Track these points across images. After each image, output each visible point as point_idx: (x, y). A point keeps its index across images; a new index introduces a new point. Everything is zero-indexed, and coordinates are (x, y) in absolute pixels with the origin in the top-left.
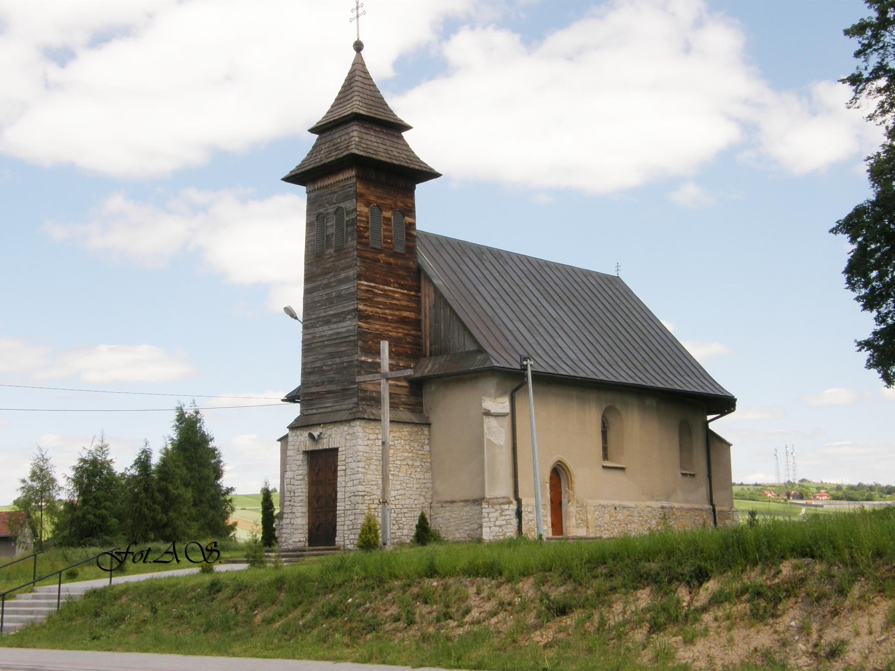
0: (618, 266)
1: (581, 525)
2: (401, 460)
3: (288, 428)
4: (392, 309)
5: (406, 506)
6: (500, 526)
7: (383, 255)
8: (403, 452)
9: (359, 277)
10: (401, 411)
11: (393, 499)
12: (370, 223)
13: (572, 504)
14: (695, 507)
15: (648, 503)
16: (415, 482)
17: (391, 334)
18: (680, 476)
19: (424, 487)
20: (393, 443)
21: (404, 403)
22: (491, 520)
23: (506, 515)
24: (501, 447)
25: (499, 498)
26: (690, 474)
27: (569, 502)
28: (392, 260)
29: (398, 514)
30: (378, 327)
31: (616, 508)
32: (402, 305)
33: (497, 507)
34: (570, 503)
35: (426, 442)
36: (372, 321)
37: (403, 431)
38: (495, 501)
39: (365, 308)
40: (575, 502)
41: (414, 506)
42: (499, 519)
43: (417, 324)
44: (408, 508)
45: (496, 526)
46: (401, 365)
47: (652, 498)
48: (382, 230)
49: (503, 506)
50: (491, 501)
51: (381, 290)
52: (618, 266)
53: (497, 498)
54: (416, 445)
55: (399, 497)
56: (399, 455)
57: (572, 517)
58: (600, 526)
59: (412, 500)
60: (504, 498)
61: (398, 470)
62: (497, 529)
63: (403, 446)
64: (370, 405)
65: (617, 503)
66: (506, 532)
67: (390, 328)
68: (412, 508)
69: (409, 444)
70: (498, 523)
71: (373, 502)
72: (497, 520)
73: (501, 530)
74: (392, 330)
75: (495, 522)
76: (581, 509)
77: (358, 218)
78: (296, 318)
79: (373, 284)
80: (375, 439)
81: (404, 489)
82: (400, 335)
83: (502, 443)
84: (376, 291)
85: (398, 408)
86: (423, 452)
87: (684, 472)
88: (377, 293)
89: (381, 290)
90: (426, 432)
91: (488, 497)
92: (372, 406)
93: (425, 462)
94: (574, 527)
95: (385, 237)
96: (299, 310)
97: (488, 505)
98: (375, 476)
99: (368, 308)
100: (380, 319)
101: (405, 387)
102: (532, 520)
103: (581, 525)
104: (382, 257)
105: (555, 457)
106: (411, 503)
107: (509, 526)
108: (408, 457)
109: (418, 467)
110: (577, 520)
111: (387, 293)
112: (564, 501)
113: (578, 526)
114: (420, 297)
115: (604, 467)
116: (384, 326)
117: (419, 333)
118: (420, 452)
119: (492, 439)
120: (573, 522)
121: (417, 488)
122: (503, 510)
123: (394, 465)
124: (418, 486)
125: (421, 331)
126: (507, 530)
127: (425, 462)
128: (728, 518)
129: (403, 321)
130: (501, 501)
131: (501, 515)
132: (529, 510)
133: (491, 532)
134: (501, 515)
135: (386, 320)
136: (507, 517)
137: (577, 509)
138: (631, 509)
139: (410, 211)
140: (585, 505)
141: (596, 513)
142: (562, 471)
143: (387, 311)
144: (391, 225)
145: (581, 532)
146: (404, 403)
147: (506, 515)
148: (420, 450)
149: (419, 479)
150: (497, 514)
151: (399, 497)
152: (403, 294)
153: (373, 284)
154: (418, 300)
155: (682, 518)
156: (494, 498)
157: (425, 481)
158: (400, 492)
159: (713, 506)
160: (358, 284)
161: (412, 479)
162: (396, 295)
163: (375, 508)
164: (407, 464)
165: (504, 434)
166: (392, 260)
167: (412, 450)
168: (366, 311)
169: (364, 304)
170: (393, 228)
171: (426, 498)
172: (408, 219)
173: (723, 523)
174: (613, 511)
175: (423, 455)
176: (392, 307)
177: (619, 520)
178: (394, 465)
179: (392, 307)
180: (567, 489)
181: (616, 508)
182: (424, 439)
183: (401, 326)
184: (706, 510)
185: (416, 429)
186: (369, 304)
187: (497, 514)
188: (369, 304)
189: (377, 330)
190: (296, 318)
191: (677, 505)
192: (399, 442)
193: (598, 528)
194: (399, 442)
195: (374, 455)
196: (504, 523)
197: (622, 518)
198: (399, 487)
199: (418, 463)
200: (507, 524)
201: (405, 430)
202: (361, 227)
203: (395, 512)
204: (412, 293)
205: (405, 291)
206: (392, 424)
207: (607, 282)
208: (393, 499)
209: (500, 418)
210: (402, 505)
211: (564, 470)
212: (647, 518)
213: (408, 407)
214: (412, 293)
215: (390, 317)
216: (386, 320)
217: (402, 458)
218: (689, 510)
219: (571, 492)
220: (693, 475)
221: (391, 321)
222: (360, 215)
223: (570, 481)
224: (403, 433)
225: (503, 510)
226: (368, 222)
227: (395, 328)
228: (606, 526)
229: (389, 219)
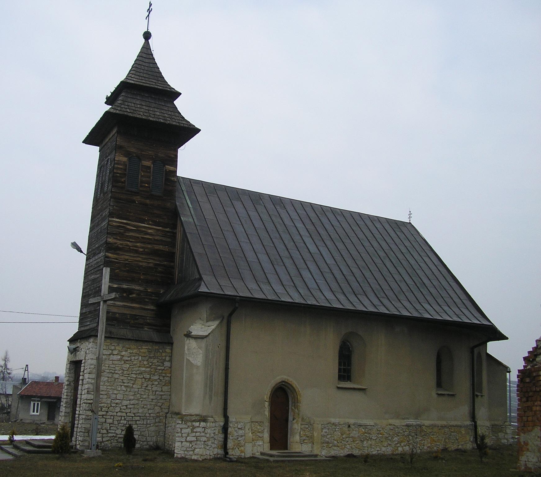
0: (410, 214)
1: (305, 441)
2: (136, 374)
3: (68, 341)
4: (144, 243)
5: (138, 414)
6: (191, 442)
7: (138, 197)
8: (139, 367)
9: (111, 215)
10: (146, 331)
11: (125, 407)
12: (127, 170)
13: (296, 422)
14: (451, 424)
15: (391, 421)
16: (151, 393)
17: (141, 264)
18: (436, 396)
19: (161, 399)
20: (129, 359)
21: (149, 324)
22: (184, 435)
23: (196, 432)
24: (198, 367)
25: (193, 415)
26: (448, 395)
27: (293, 420)
28: (148, 201)
29: (128, 421)
30: (127, 257)
31: (349, 426)
32: (155, 240)
33: (189, 424)
34: (295, 421)
35: (168, 358)
36: (121, 253)
37: (142, 349)
38: (188, 418)
39: (115, 241)
40: (300, 420)
41: (147, 415)
42: (190, 435)
43: (171, 256)
44: (140, 417)
45: (186, 441)
46: (149, 290)
47: (397, 416)
48: (140, 176)
49: (194, 423)
50: (185, 418)
51: (134, 226)
52: (410, 214)
53: (191, 415)
54: (155, 361)
55: (131, 406)
56: (135, 369)
57: (296, 433)
58: (328, 443)
59: (146, 409)
60: (197, 415)
61: (132, 382)
62: (188, 444)
63: (140, 362)
64: (112, 325)
65: (352, 421)
66: (195, 448)
67: (140, 259)
68: (145, 416)
69: (147, 360)
70: (188, 439)
71: (102, 409)
72: (188, 436)
73: (191, 446)
74: (142, 260)
75: (186, 437)
76: (307, 426)
77: (116, 166)
78: (82, 252)
79: (125, 221)
80: (110, 355)
81: (138, 400)
82: (151, 265)
83: (199, 364)
84: (128, 227)
85: (142, 328)
86: (163, 368)
87: (440, 392)
88: (128, 228)
89: (134, 226)
90: (168, 350)
91: (184, 414)
92: (114, 325)
93: (164, 377)
94: (297, 442)
95: (142, 182)
96: (84, 246)
97: (182, 421)
98: (105, 387)
99: (118, 241)
100: (130, 250)
101: (152, 310)
102: (242, 436)
103: (305, 441)
104: (137, 199)
105: (278, 378)
106: (145, 412)
107: (198, 442)
108: (145, 372)
109: (156, 380)
110: (300, 437)
111: (139, 229)
112: (290, 418)
113: (302, 442)
114: (176, 233)
115: (338, 388)
116: (133, 257)
117: (172, 264)
118: (159, 368)
119: (191, 359)
120: (297, 438)
121: (152, 399)
122: (194, 427)
123: (129, 378)
124: (154, 397)
125: (174, 262)
126: (196, 447)
127: (164, 377)
128: (501, 431)
129: (155, 253)
130: (193, 418)
131: (192, 432)
132: (239, 427)
133: (182, 447)
134: (192, 432)
135: (137, 252)
136: (198, 434)
137: (302, 427)
138: (368, 427)
139: (174, 161)
140: (312, 422)
141: (324, 431)
142: (288, 390)
143: (138, 244)
144: (150, 172)
145: (305, 449)
146: (149, 324)
147: (196, 432)
148: (159, 366)
149: (156, 391)
150: (189, 430)
151: (131, 406)
152: (158, 230)
153: (125, 221)
154: (174, 236)
155: (433, 435)
156: (188, 415)
157: (163, 394)
158: (132, 402)
159: (475, 423)
160: (109, 221)
161: (147, 391)
162: (150, 231)
163: (103, 415)
164: (144, 378)
165: (201, 355)
166: (148, 201)
167: (151, 366)
168: (116, 243)
169: (114, 238)
170: (152, 174)
171: (162, 409)
172: (169, 168)
173: (497, 435)
174: (346, 429)
175: (163, 370)
176: (144, 241)
177: (352, 437)
178: (129, 378)
179: (144, 241)
180: (293, 408)
181: (349, 426)
182: (166, 356)
183: (152, 258)
184: (466, 426)
185: (157, 347)
186: (118, 238)
187: (189, 430)
188: (118, 238)
189: (127, 260)
190: (82, 252)
191: (427, 423)
192: (136, 358)
193: (325, 445)
194: (136, 358)
195: (107, 368)
196: (194, 439)
197: (356, 436)
198: (132, 397)
199: (156, 377)
200: (197, 441)
201: (144, 347)
202: (118, 173)
203: (125, 419)
204: (168, 229)
205: (160, 228)
206: (108, 341)
207: (378, 225)
208: (125, 407)
209: (199, 340)
210: (134, 414)
211: (289, 388)
212: (387, 436)
213: (154, 327)
214: (168, 229)
215: (141, 250)
216: (137, 252)
217: (138, 372)
218: (443, 427)
219: (296, 410)
220: (453, 395)
221: (142, 253)
222: (118, 164)
223: (296, 401)
224: (142, 351)
225: (194, 427)
226: (125, 170)
227: (145, 259)
228: (336, 442)
229: (149, 168)
